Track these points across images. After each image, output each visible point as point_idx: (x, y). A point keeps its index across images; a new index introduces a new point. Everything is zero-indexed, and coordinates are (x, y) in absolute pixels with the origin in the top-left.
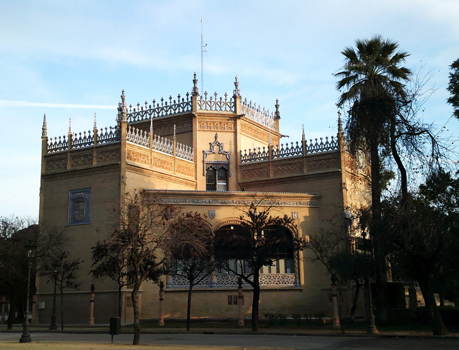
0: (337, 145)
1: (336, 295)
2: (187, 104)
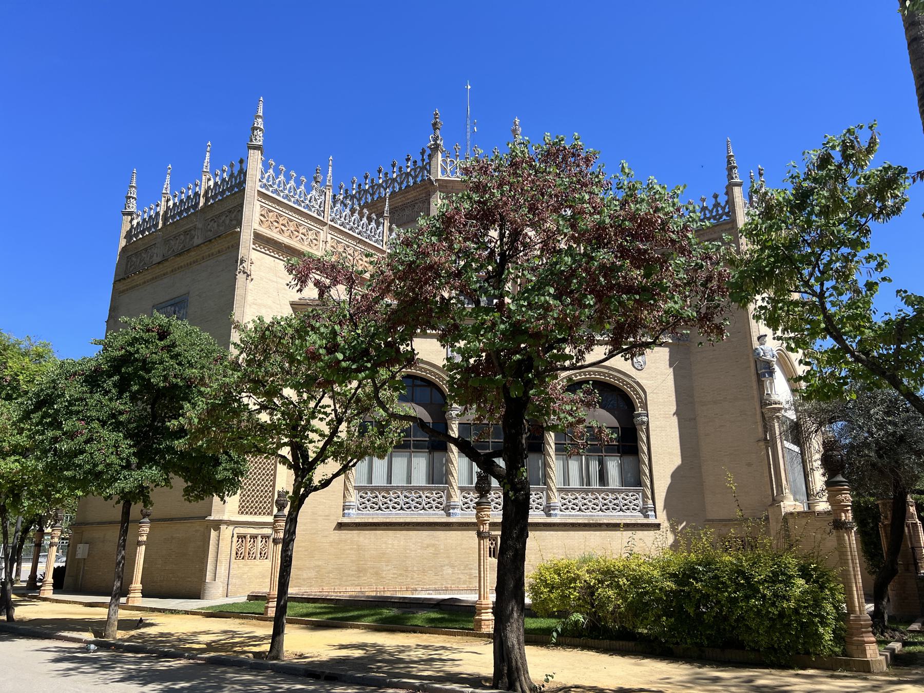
0: (727, 210)
1: (739, 185)
2: (423, 168)
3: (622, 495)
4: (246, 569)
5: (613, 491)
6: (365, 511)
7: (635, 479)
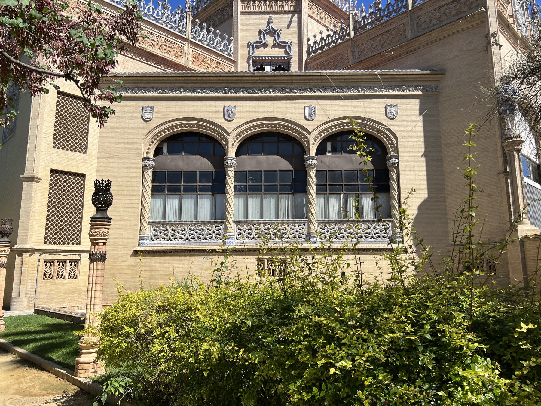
3: (374, 225)
4: (54, 287)
5: (366, 222)
6: (157, 241)
7: (384, 212)
